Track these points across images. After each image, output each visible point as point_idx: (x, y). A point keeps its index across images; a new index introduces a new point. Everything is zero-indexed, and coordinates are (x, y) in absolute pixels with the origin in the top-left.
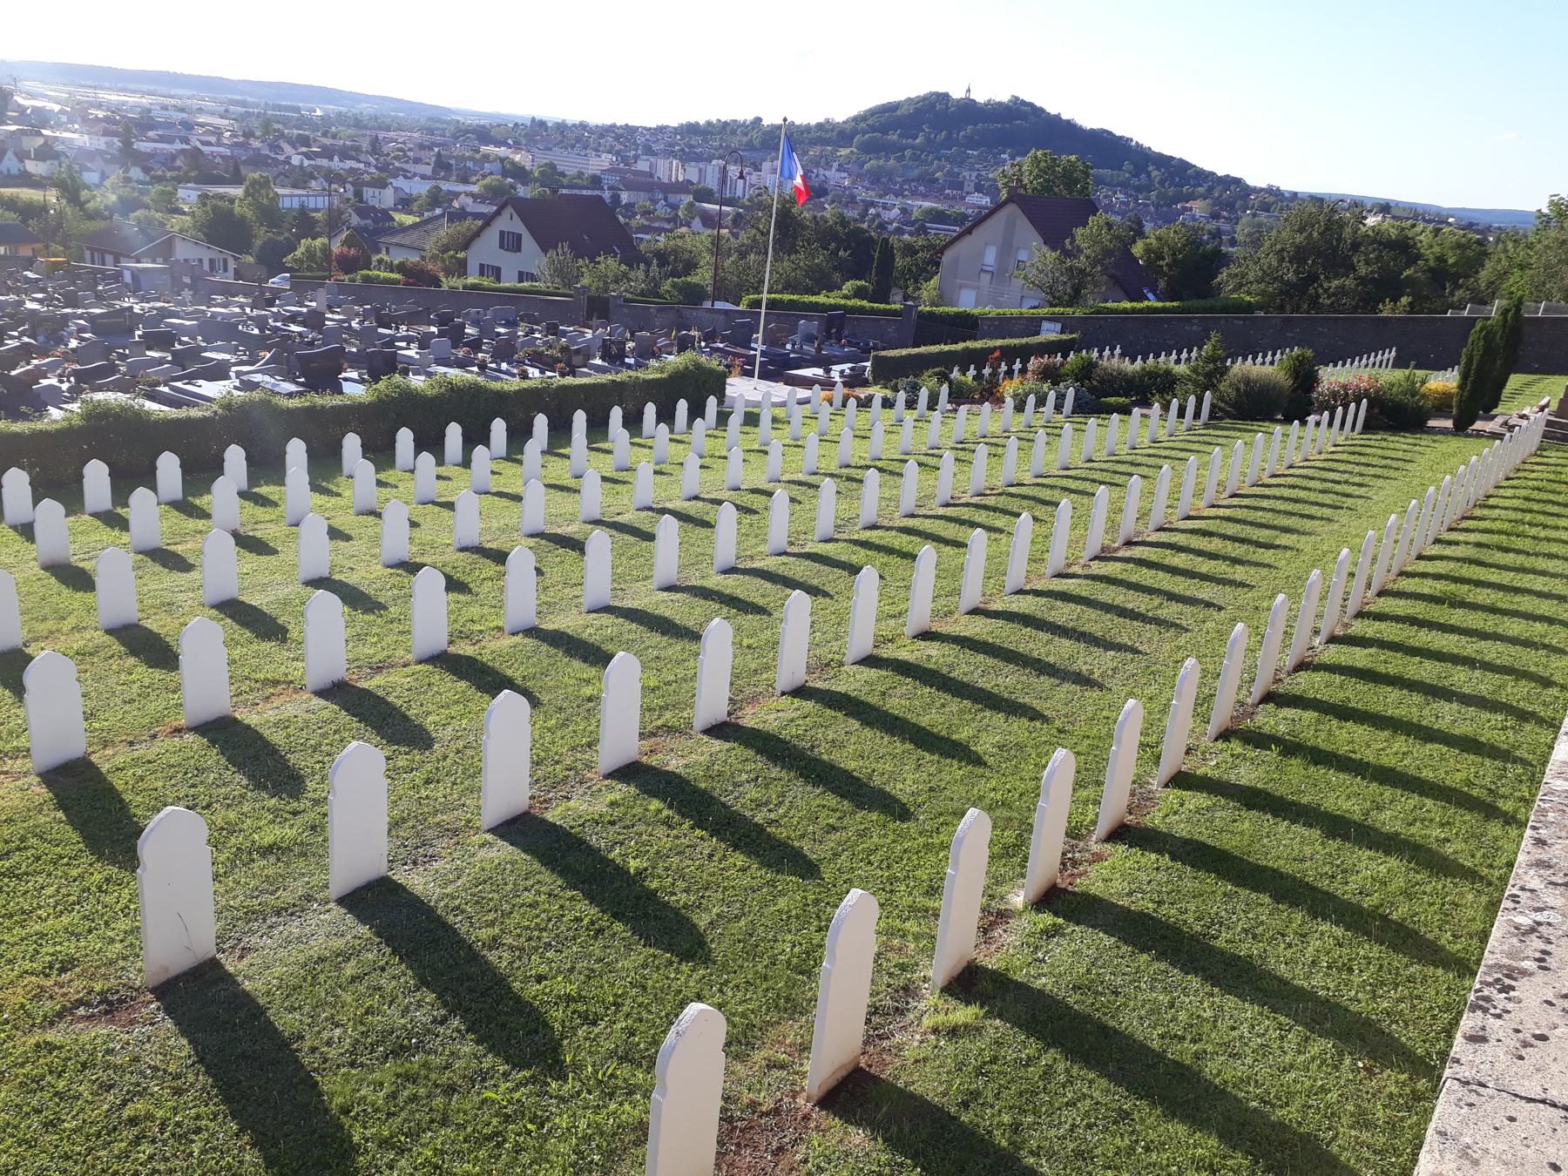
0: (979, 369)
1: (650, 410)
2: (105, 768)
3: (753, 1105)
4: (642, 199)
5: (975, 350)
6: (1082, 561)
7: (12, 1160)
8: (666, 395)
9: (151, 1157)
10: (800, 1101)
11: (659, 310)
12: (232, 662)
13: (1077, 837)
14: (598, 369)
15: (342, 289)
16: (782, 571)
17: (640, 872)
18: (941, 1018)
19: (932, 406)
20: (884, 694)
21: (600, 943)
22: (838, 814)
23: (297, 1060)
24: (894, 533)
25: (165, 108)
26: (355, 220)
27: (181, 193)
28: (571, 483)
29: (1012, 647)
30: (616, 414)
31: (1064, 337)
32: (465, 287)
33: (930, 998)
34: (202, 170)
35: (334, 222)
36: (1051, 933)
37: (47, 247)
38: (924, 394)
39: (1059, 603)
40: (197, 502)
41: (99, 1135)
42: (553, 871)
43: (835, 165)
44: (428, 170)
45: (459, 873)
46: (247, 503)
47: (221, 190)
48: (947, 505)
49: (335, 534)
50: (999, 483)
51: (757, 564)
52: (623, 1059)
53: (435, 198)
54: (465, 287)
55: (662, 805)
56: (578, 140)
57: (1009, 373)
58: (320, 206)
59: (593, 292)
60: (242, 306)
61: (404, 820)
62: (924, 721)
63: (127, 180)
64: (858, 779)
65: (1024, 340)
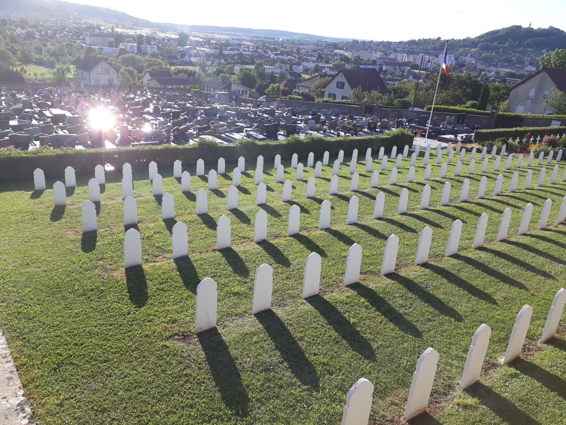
0: (521, 139)
1: (382, 149)
2: (192, 259)
3: (384, 416)
4: (391, 69)
5: (520, 131)
6: (555, 224)
7: (152, 380)
8: (388, 145)
9: (190, 388)
10: (402, 419)
11: (392, 111)
12: (233, 229)
13: (533, 339)
14: (365, 132)
15: (282, 101)
16: (425, 216)
17: (354, 324)
18: (461, 400)
19: (498, 153)
20: (459, 270)
21: (337, 346)
22: (432, 315)
23: (235, 366)
24: (474, 205)
25: (233, 39)
26: (289, 77)
27: (235, 68)
28: (349, 176)
29: (517, 257)
30: (369, 151)
31: (562, 127)
32: (323, 102)
33: (458, 392)
34: (242, 60)
35: (282, 77)
36: (513, 376)
37: (194, 85)
38: (495, 148)
39: (541, 241)
40: (229, 174)
41: (176, 378)
42: (324, 317)
43: (469, 55)
44: (315, 59)
45: (293, 312)
46: (244, 176)
47: (247, 67)
48: (498, 195)
49: (269, 189)
50: (523, 188)
51: (415, 213)
52: (340, 389)
53: (317, 69)
54: (323, 102)
55: (365, 301)
56: (369, 47)
57: (534, 142)
58: (278, 71)
59: (368, 104)
60: (250, 107)
61: (278, 290)
62: (474, 283)
63: (220, 63)
64: (443, 303)
65: (543, 128)
